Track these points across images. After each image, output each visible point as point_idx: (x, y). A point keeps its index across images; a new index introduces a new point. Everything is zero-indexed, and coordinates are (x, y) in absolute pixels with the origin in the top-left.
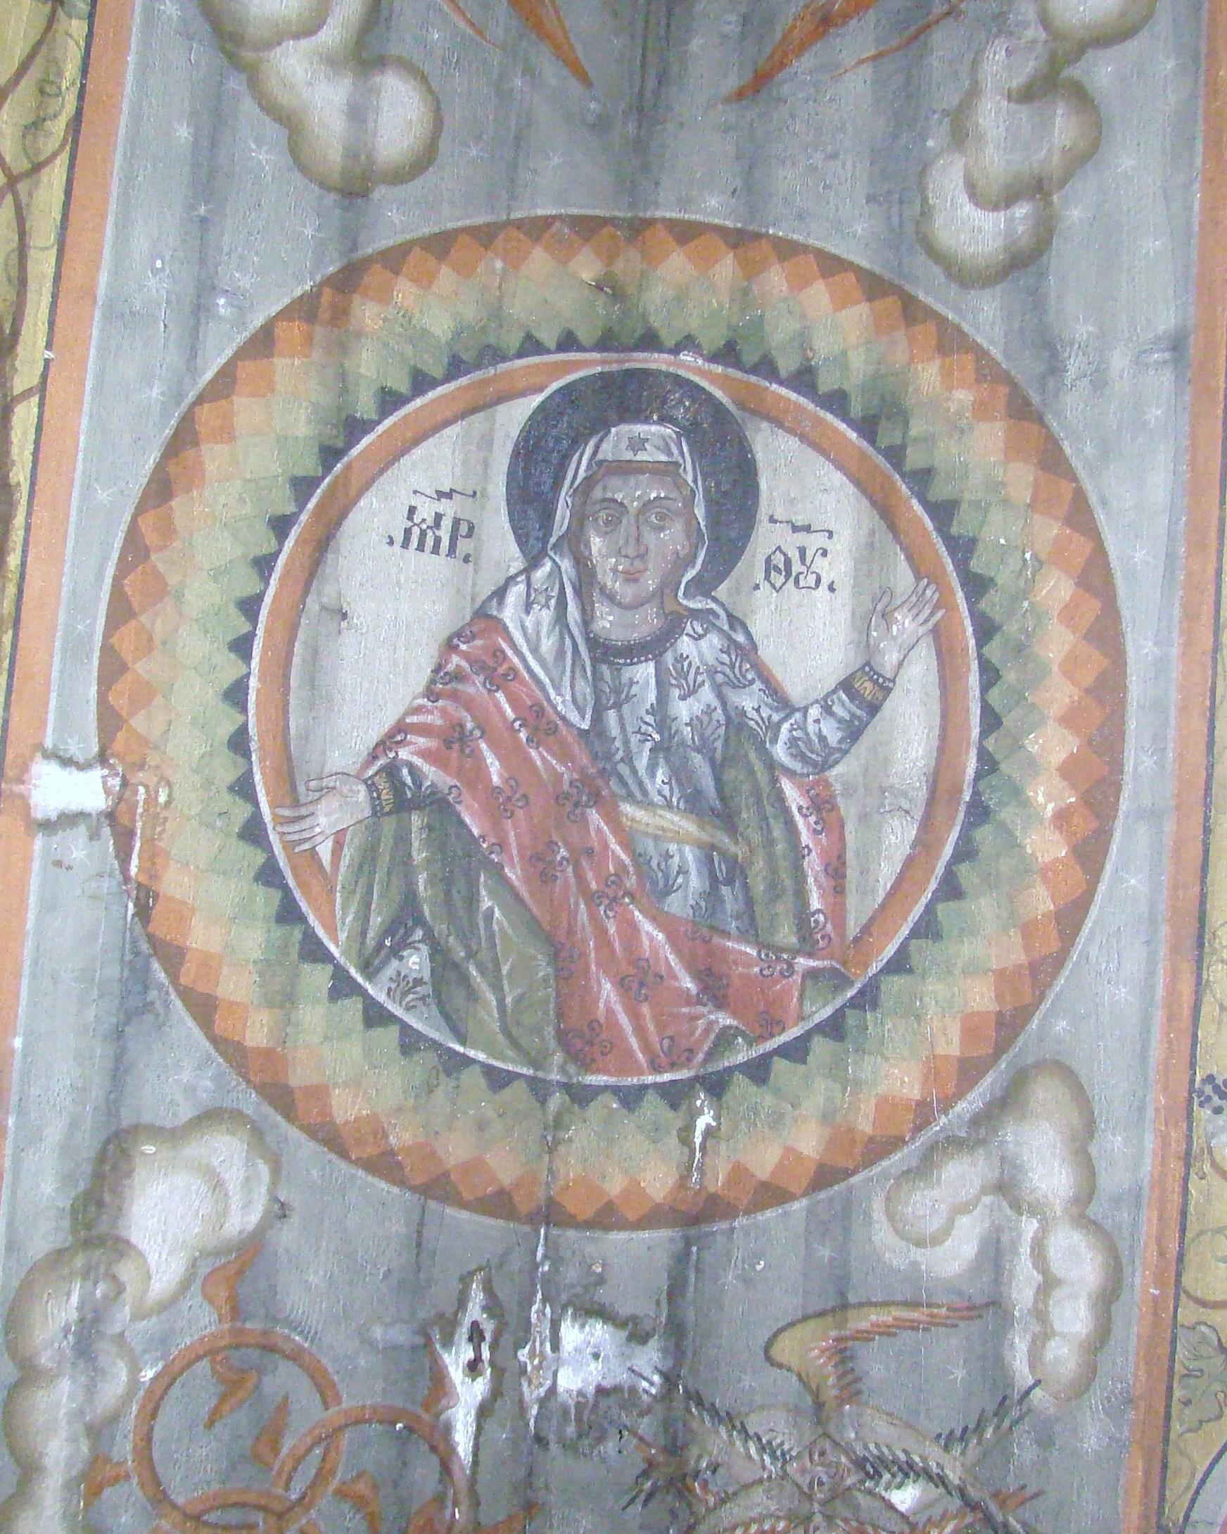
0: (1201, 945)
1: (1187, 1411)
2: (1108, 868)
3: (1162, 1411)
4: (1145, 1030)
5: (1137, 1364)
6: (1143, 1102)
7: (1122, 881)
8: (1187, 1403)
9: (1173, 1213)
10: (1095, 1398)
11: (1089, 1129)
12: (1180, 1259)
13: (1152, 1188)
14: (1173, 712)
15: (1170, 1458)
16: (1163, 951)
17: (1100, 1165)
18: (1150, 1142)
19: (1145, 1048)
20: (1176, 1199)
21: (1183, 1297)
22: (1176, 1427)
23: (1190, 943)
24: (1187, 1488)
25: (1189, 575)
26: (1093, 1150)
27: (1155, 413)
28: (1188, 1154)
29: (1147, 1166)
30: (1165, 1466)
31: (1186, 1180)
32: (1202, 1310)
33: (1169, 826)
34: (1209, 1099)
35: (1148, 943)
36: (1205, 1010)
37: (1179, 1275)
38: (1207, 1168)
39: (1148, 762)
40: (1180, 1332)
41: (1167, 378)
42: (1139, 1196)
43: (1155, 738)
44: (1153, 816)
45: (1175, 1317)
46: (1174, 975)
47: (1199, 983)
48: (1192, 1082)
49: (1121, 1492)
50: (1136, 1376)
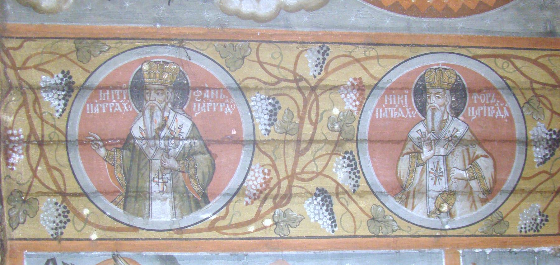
0: (369, 44)
1: (222, 47)
2: (392, 14)
3: (221, 38)
4: (341, 27)
5: (235, 29)
6: (320, 27)
7: (388, 18)
8: (225, 47)
9: (284, 39)
10: (222, 16)
11: (310, 10)
12: (270, 42)
13: (291, 31)
14: (440, 33)
15: (206, 42)
16: (367, 32)
17: (298, 14)
18: (307, 30)
19: (337, 27)
20: (289, 39)
21: (258, 43)
22: (216, 44)
23: (370, 41)
24: (197, 49)
25: (482, 37)
26: (303, 11)
27: (531, 26)
28: (304, 43)
29: (299, 29)
30: (203, 40)
31: (296, 42)
32: (255, 50)
33: (405, 33)
34: (322, 49)
35: (369, 27)
36: (350, 46)
37: (265, 41)
38: (300, 49)
39: (425, 26)
40: (247, 43)
41: (542, 30)
42: (288, 27)
43: (433, 28)
44: (409, 28)
45: (252, 41)
46: (359, 36)
47: (358, 44)
48: (327, 43)
49: (192, 26)
50: (230, 29)
